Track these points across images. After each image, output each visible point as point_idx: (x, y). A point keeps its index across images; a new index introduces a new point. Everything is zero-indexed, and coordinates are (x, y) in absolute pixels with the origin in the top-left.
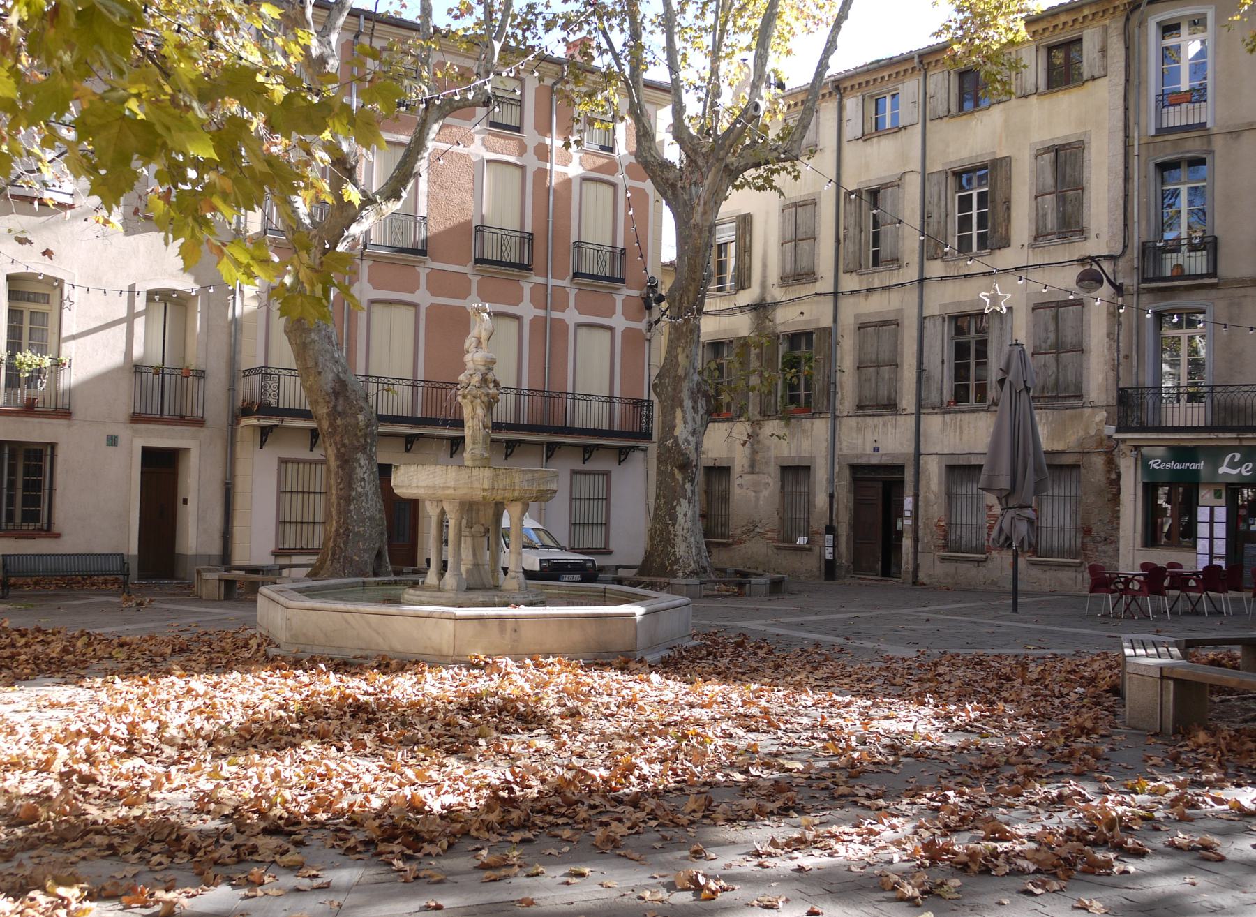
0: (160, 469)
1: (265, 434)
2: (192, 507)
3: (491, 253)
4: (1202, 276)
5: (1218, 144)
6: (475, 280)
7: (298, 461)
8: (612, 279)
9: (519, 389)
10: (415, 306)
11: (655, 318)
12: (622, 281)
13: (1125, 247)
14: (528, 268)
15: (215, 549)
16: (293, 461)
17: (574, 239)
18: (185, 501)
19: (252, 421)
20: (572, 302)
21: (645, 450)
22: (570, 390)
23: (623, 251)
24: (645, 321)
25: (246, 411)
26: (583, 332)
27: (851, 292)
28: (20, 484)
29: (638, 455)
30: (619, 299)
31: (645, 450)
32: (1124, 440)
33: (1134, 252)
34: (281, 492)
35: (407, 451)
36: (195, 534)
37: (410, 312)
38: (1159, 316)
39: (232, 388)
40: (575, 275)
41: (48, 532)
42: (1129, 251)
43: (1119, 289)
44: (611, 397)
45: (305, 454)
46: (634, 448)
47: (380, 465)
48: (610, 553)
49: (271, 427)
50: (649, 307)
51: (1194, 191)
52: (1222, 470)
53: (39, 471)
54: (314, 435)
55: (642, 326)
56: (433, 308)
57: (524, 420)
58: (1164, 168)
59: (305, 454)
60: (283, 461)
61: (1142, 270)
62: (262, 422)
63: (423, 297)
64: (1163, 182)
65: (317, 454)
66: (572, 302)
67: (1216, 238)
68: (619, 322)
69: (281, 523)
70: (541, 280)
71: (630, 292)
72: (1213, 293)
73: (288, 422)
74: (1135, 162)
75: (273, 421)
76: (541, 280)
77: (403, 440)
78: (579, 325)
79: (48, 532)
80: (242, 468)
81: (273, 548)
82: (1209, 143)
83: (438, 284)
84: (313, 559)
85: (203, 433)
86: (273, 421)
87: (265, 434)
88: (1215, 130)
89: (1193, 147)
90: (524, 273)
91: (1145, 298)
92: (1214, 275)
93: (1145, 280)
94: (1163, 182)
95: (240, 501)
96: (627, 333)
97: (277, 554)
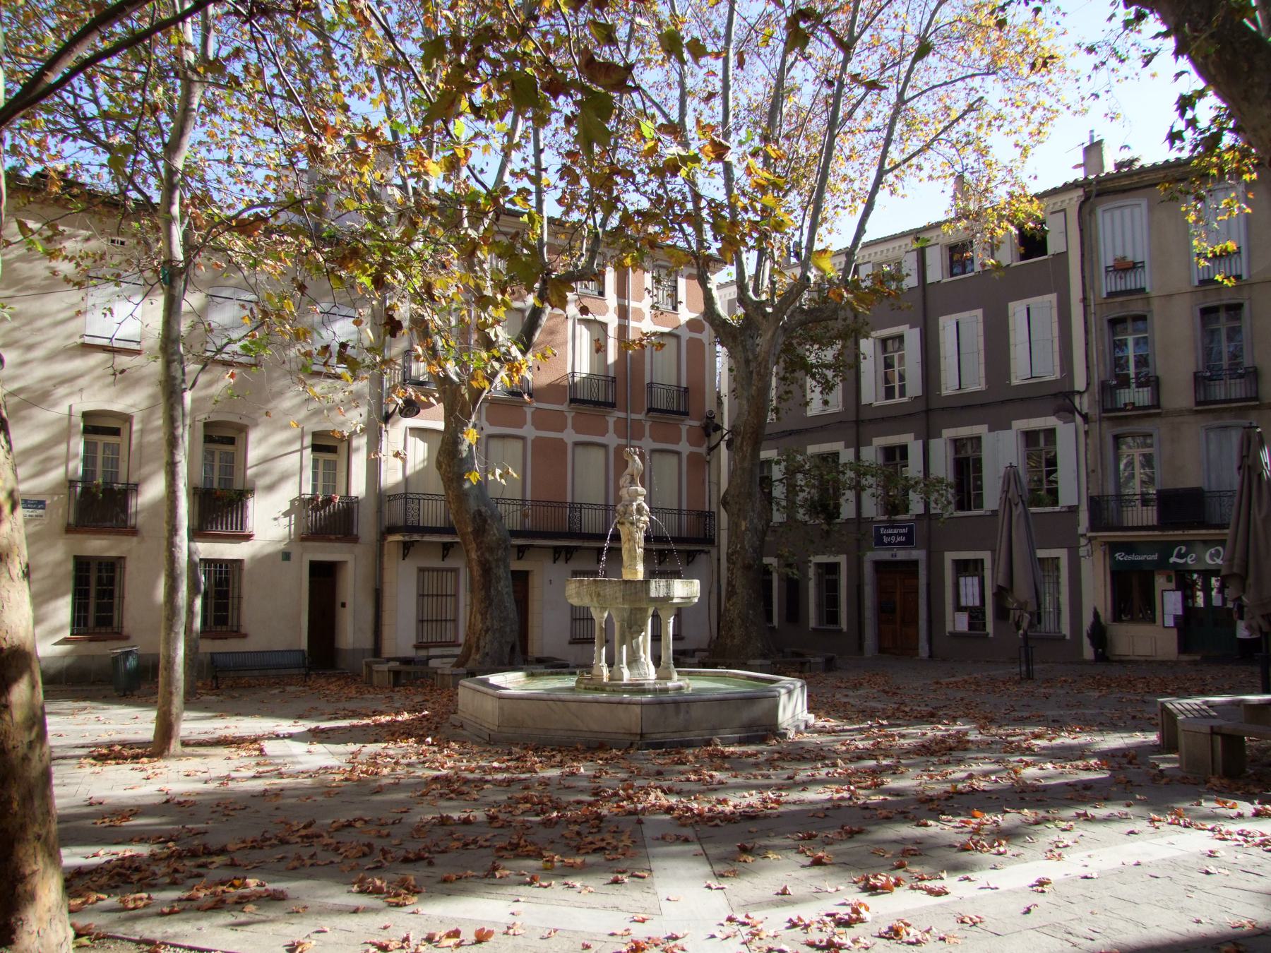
0: (324, 577)
1: (407, 548)
2: (349, 607)
3: (661, 403)
4: (1144, 408)
5: (1156, 305)
6: (570, 416)
7: (433, 570)
8: (678, 413)
9: (680, 510)
10: (523, 438)
11: (713, 443)
12: (686, 414)
13: (1088, 384)
14: (613, 405)
15: (368, 643)
16: (428, 570)
17: (647, 381)
18: (343, 605)
19: (398, 538)
20: (569, 421)
21: (708, 552)
22: (569, 500)
23: (686, 390)
24: (705, 446)
25: (392, 530)
26: (579, 450)
27: (870, 420)
28: (93, 593)
29: (703, 556)
30: (684, 429)
31: (708, 552)
32: (1095, 538)
33: (1095, 387)
34: (421, 596)
35: (519, 558)
36: (352, 631)
37: (519, 444)
38: (1117, 438)
39: (379, 510)
40: (650, 410)
41: (239, 634)
42: (1091, 387)
43: (1085, 418)
44: (680, 510)
45: (437, 563)
46: (702, 551)
47: (513, 572)
48: (245, 636)
49: (413, 543)
50: (708, 435)
51: (1137, 342)
52: (1172, 560)
53: (111, 581)
54: (446, 549)
55: (702, 450)
56: (538, 439)
57: (684, 534)
58: (1114, 323)
59: (437, 563)
60: (421, 570)
61: (1102, 401)
62: (407, 539)
63: (529, 431)
64: (1114, 334)
65: (449, 563)
66: (569, 421)
67: (1157, 378)
68: (685, 447)
69: (421, 621)
70: (622, 415)
71: (690, 424)
72: (1157, 420)
73: (428, 538)
74: (1092, 319)
75: (416, 537)
76: (622, 415)
77: (552, 551)
78: (576, 444)
79: (239, 634)
80: (388, 577)
81: (414, 642)
82: (1149, 304)
83: (541, 420)
84: (458, 651)
85: (358, 549)
86: (416, 537)
87: (407, 548)
88: (1153, 294)
89: (1137, 308)
90: (609, 410)
91: (1105, 425)
92: (1158, 406)
93: (1105, 411)
94: (1114, 334)
95: (387, 604)
96: (692, 456)
97: (418, 647)
